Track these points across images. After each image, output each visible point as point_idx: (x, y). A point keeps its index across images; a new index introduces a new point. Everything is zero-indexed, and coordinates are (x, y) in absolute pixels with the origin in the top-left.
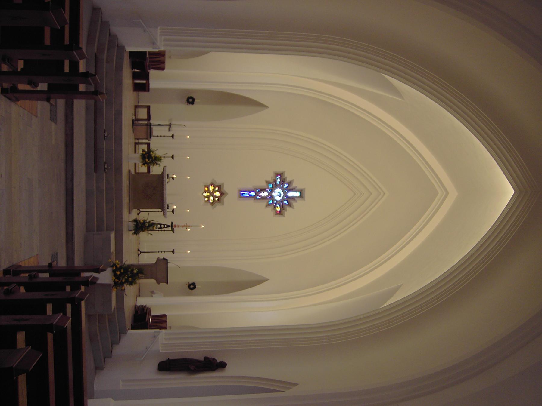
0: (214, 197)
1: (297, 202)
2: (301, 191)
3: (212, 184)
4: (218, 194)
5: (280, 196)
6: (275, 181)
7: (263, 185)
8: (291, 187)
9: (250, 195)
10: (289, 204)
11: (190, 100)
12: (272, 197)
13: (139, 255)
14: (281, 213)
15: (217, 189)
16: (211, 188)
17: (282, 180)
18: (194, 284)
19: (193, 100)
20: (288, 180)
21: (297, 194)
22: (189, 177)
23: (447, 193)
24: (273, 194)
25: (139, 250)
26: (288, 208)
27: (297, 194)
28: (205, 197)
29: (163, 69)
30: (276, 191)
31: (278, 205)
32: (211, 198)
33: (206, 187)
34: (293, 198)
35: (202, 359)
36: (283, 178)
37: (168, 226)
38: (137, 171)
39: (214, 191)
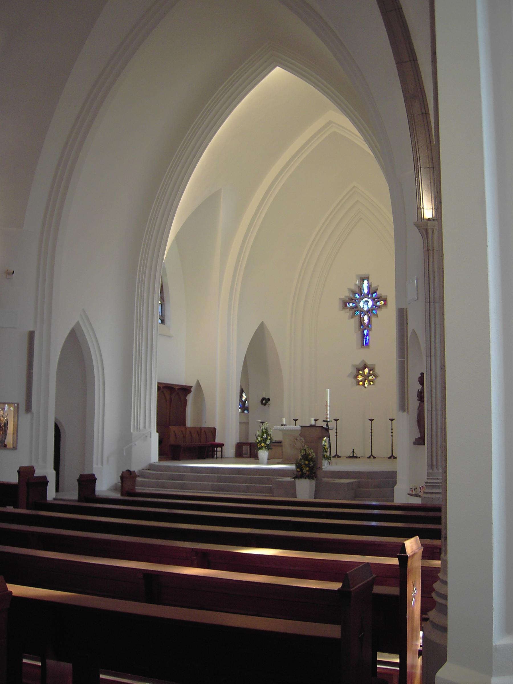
0: (369, 375)
2: (362, 280)
3: (356, 377)
4: (366, 371)
5: (368, 302)
6: (352, 308)
8: (357, 290)
9: (367, 336)
11: (264, 402)
12: (369, 311)
13: (374, 458)
14: (385, 300)
15: (361, 372)
16: (360, 378)
17: (351, 304)
19: (264, 399)
20: (379, 313)
21: (366, 282)
26: (379, 292)
28: (370, 384)
29: (214, 429)
30: (362, 307)
31: (378, 304)
33: (359, 384)
34: (369, 288)
36: (347, 299)
39: (363, 375)
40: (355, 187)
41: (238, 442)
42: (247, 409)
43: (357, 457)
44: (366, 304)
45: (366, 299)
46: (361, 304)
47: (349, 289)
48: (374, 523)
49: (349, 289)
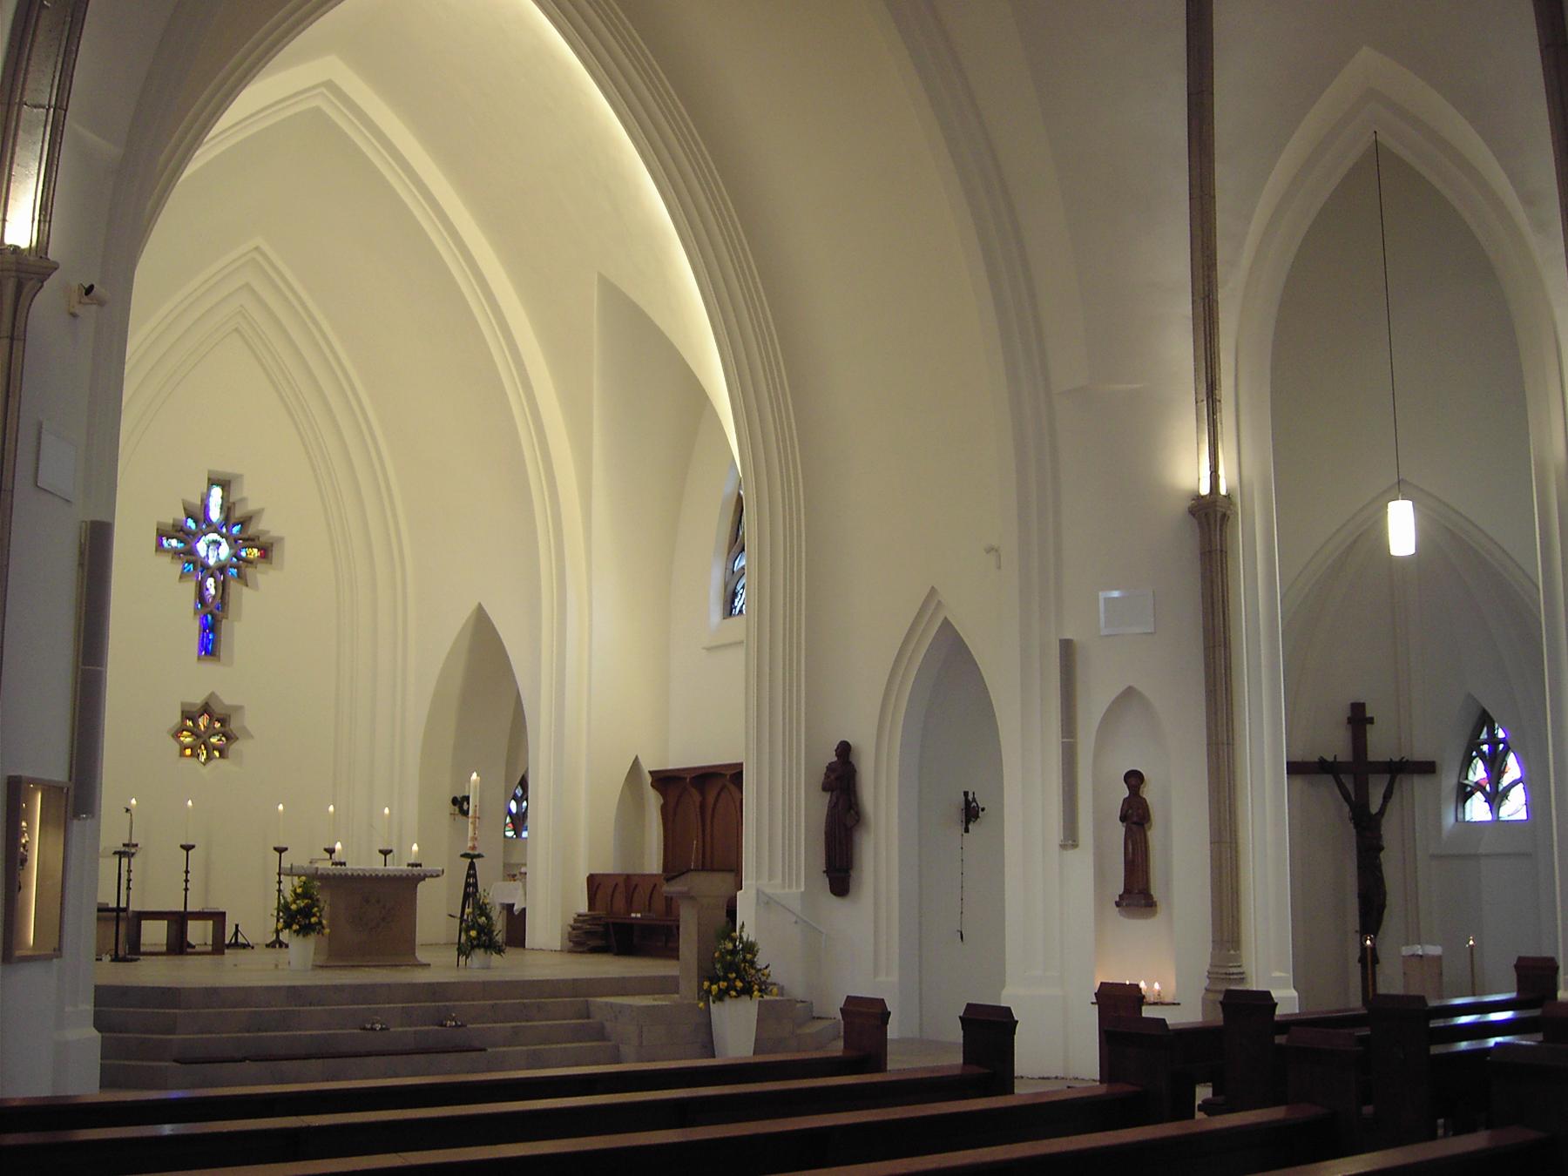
1: (243, 500)
3: (176, 735)
6: (176, 553)
7: (190, 587)
10: (244, 522)
12: (222, 568)
14: (266, 551)
18: (455, 801)
22: (281, 807)
23: (330, 85)
24: (212, 562)
25: (271, 945)
27: (217, 492)
28: (209, 758)
30: (203, 553)
32: (214, 740)
34: (227, 508)
35: (827, 796)
37: (472, 866)
38: (164, 949)
39: (194, 733)
40: (257, 248)
41: (608, 865)
42: (455, 801)
43: (245, 946)
44: (213, 550)
45: (214, 536)
46: (201, 547)
47: (260, 512)
48: (167, 1129)
49: (260, 512)
